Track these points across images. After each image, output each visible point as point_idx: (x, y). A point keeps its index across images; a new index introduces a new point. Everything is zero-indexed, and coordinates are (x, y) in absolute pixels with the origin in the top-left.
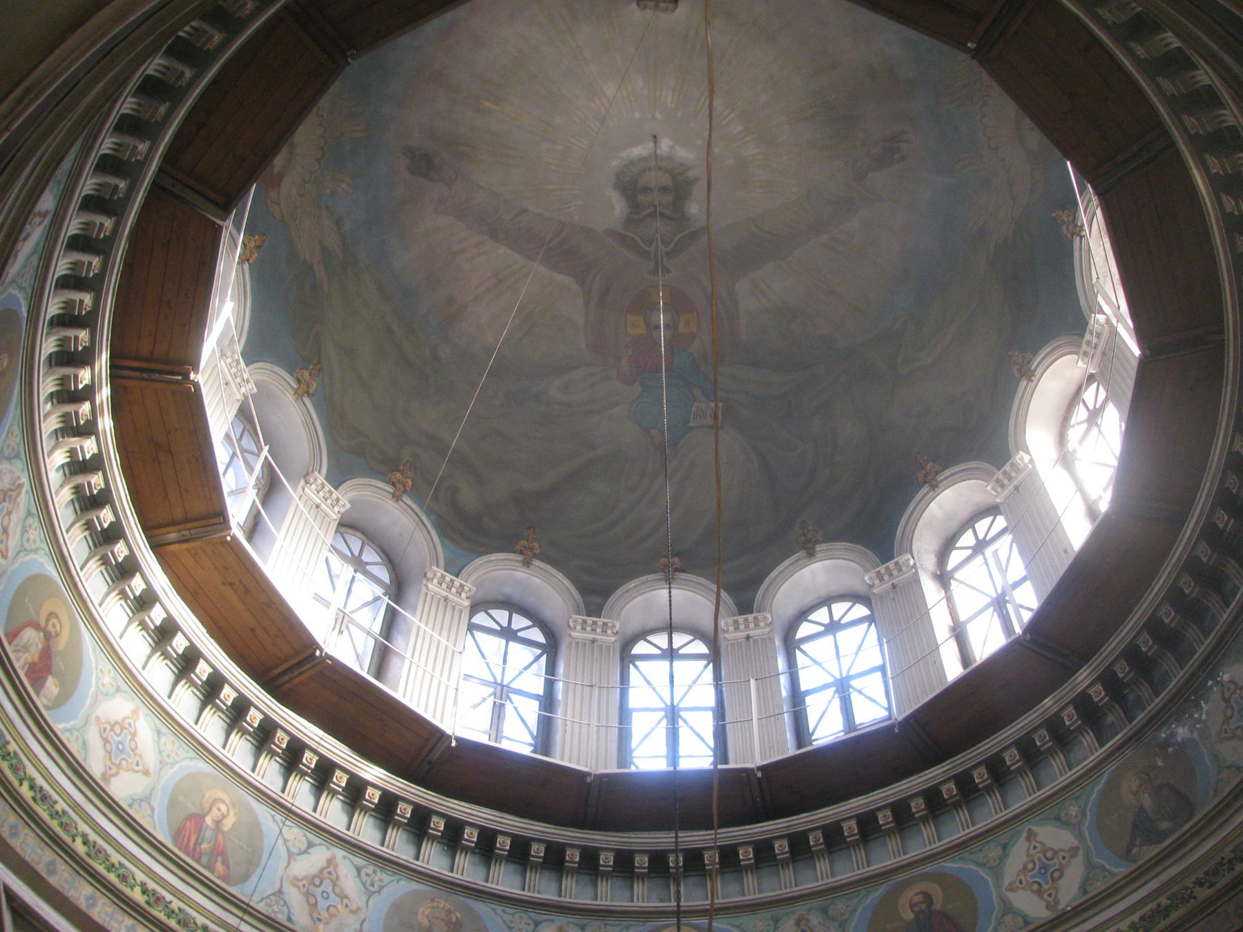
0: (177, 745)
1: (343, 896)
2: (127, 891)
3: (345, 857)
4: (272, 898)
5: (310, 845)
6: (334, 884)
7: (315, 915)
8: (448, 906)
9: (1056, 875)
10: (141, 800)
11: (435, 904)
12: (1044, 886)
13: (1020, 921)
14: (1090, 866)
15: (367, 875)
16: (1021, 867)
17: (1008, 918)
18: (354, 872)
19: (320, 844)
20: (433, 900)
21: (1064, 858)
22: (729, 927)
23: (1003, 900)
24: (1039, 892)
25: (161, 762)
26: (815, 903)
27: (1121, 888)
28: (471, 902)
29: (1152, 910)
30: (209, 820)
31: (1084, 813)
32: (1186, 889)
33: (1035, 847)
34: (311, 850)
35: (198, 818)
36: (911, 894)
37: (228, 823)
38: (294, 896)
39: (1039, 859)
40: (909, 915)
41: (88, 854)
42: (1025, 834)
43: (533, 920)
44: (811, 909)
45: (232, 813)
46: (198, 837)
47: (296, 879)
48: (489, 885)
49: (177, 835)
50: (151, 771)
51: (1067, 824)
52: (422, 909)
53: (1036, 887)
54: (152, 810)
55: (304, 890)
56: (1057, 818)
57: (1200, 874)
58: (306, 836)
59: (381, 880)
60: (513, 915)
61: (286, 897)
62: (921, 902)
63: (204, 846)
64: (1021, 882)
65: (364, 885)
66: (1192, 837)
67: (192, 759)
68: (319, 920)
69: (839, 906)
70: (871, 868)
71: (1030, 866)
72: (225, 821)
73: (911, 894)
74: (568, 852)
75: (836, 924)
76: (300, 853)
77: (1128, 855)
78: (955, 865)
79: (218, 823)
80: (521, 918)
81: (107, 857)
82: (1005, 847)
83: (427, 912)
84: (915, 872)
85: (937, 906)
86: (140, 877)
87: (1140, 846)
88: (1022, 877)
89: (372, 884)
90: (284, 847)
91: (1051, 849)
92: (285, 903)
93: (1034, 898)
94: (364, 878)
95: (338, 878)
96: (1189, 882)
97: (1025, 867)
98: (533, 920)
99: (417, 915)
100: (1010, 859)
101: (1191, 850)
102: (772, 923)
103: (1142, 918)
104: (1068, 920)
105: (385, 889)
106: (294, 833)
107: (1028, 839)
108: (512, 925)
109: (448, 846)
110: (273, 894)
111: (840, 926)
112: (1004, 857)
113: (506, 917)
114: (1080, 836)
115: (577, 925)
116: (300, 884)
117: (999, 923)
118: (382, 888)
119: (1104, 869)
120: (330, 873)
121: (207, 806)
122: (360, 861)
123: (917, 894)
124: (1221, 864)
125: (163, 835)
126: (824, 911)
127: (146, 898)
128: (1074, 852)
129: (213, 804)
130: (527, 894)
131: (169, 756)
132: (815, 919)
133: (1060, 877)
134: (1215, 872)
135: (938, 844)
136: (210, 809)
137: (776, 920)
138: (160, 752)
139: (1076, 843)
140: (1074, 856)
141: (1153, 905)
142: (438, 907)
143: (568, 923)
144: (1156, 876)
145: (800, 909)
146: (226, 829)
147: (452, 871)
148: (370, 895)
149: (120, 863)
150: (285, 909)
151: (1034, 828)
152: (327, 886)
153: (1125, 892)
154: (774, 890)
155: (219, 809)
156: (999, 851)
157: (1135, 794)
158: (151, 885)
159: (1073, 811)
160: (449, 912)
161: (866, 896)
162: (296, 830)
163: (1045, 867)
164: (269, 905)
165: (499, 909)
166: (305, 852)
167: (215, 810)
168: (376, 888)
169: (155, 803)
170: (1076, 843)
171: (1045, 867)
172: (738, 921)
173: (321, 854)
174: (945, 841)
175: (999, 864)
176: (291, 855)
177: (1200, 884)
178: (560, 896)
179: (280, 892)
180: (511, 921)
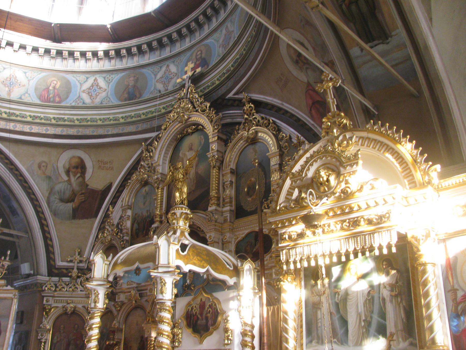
0: (33, 73)
2: (25, 120)
5: (87, 78)
6: (97, 86)
8: (134, 75)
10: (24, 94)
18: (103, 79)
25: (28, 80)
30: (51, 88)
34: (88, 80)
35: (47, 89)
37: (58, 86)
41: (8, 116)
45: (58, 82)
46: (48, 94)
49: (40, 97)
63: (51, 96)
65: (107, 82)
67: (40, 74)
70: (171, 53)
72: (56, 86)
76: (85, 82)
79: (54, 88)
80: (156, 68)
81: (15, 114)
86: (28, 114)
90: (79, 83)
92: (81, 99)
95: (98, 84)
121: (49, 85)
125: (38, 102)
127: (32, 118)
129: (51, 83)
131: (31, 77)
136: (50, 85)
138: (27, 78)
152: (95, 87)
155: (54, 83)
162: (82, 76)
165: (150, 68)
166: (86, 81)
170: (106, 88)
174: (162, 57)
176: (81, 85)
179: (79, 96)
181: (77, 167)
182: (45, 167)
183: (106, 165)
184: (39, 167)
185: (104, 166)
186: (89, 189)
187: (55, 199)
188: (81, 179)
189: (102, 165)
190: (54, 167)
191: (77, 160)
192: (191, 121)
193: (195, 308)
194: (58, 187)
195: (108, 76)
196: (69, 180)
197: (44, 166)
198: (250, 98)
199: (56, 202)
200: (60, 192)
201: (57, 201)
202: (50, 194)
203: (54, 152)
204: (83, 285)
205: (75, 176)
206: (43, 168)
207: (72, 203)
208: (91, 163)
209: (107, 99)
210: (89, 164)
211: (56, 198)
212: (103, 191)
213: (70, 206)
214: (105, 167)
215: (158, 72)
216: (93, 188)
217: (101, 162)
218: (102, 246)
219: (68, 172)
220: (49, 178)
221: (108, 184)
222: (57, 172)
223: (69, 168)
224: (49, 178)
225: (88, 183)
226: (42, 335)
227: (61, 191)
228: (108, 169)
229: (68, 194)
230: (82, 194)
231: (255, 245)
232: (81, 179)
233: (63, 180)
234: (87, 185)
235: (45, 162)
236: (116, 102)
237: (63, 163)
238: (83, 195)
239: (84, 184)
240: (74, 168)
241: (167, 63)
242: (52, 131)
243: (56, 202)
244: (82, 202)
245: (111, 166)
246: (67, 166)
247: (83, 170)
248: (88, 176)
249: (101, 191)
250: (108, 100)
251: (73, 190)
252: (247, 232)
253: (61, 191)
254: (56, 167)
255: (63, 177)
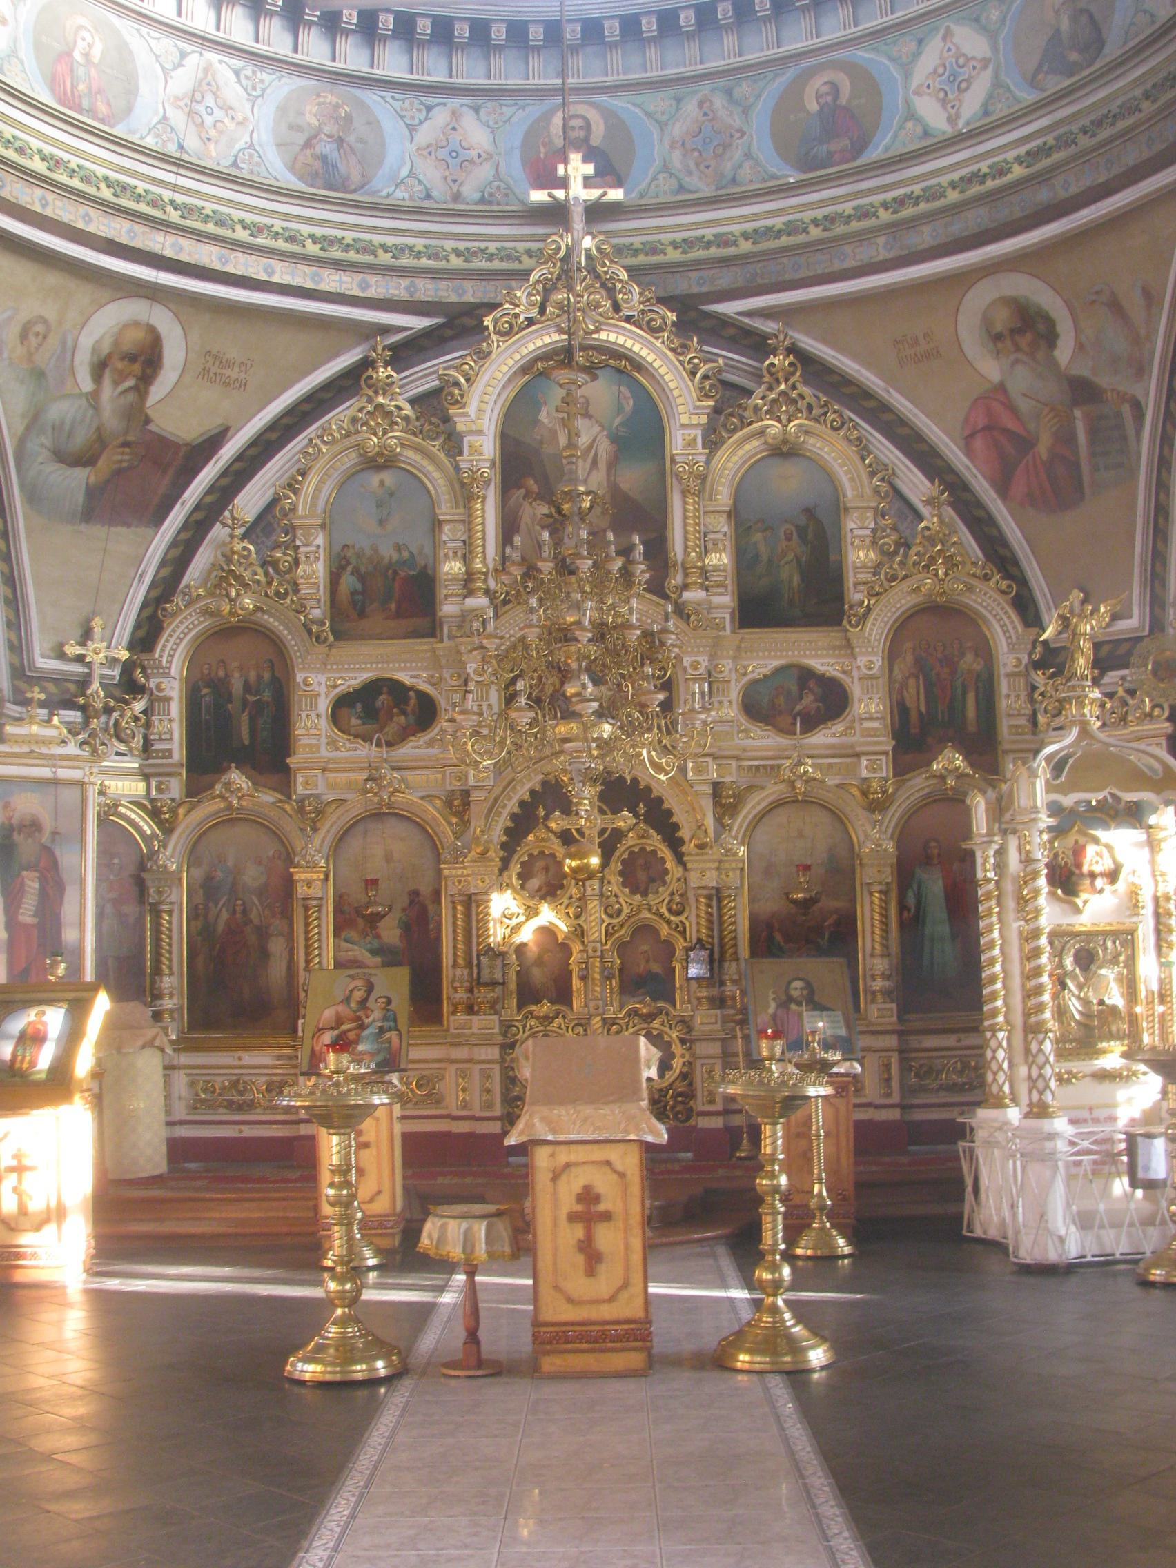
1: (227, 108)
3: (220, 62)
4: (159, 126)
5: (183, 55)
7: (204, 135)
8: (335, 100)
9: (964, 85)
10: (9, 56)
11: (322, 100)
12: (951, 96)
13: (919, 130)
14: (997, 84)
15: (247, 78)
16: (931, 70)
17: (909, 125)
19: (194, 52)
20: (318, 95)
21: (974, 68)
22: (629, 106)
23: (907, 103)
24: (944, 102)
26: (720, 83)
27: (1016, 119)
28: (358, 92)
29: (1038, 147)
30: (77, 56)
31: (1003, 21)
32: (1072, 133)
33: (949, 50)
36: (818, 83)
38: (178, 118)
39: (940, 83)
40: (813, 107)
42: (942, 31)
43: (424, 104)
44: (716, 89)
45: (97, 39)
47: (177, 99)
48: (375, 71)
50: (7, 17)
51: (984, 29)
52: (308, 108)
53: (942, 95)
54: (22, 63)
55: (187, 110)
56: (977, 20)
57: (1086, 122)
58: (176, 46)
59: (262, 81)
60: (403, 100)
61: (172, 122)
62: (827, 94)
64: (928, 87)
65: (246, 90)
66: (1091, 81)
68: (209, 140)
69: (743, 90)
71: (941, 70)
73: (818, 83)
74: (457, 26)
75: (740, 109)
76: (175, 68)
77: (1033, 83)
78: (866, 55)
80: (412, 104)
82: (920, 42)
83: (314, 111)
84: (824, 58)
85: (843, 100)
87: (1047, 73)
88: (930, 82)
89: (254, 89)
91: (964, 55)
93: (937, 107)
94: (244, 82)
95: (218, 88)
96: (1074, 128)
97: (935, 71)
98: (424, 104)
99: (304, 115)
100: (923, 57)
101: (1087, 94)
102: (674, 103)
103: (1028, 153)
104: (962, 141)
105: (268, 91)
106: (167, 45)
107: (944, 39)
108: (403, 113)
109: (326, 28)
110: (159, 122)
111: (743, 112)
112: (917, 55)
113: (397, 105)
114: (995, 48)
115: (470, 107)
116: (182, 104)
117: (901, 128)
118: (264, 90)
119: (1009, 89)
120: (209, 84)
122: (237, 63)
123: (826, 83)
124: (1106, 116)
126: (729, 92)
128: (985, 63)
130: (417, 77)
132: (719, 102)
133: (967, 89)
134: (1099, 123)
135: (853, 30)
136: (75, 42)
137: (679, 100)
139: (989, 54)
140: (985, 68)
141: (1039, 142)
142: (324, 103)
143: (462, 105)
144: (1050, 112)
145: (705, 88)
146: (96, 60)
147: (334, 60)
148: (253, 100)
149: (14, 137)
150: (174, 135)
151: (953, 27)
153: (1020, 122)
154: (677, 66)
155: (84, 39)
156: (913, 45)
157: (1057, 12)
158: (48, 149)
159: (995, 15)
160: (337, 106)
161: (774, 79)
163: (954, 75)
164: (157, 136)
165: (388, 95)
166: (180, 65)
167: (79, 42)
168: (259, 92)
169: (22, 55)
170: (989, 54)
171: (954, 75)
172: (638, 99)
173: (197, 59)
175: (911, 63)
177: (1084, 131)
178: (451, 77)
179: (165, 118)
180: (402, 109)
181: (132, 358)
182: (40, 337)
183: (227, 372)
184: (24, 336)
185: (219, 371)
186: (151, 432)
187: (40, 445)
188: (131, 397)
189: (215, 369)
190: (64, 343)
191: (139, 335)
192: (598, 340)
193: (1061, 856)
194: (61, 410)
195: (249, 72)
196: (95, 395)
197: (37, 334)
198: (793, 344)
199: (40, 459)
200: (57, 428)
201: (44, 454)
202: (28, 429)
203: (83, 294)
204: (123, 736)
205: (116, 383)
206: (33, 341)
207: (88, 469)
208: (183, 354)
209: (251, 156)
210: (174, 354)
211: (42, 445)
212: (194, 447)
213: (80, 476)
214: (221, 375)
215: (421, 123)
216: (164, 434)
217: (215, 357)
218: (200, 623)
219: (100, 368)
220: (39, 375)
221: (217, 431)
222: (68, 362)
223: (109, 356)
224: (39, 375)
225: (149, 412)
226: (160, 893)
227: (62, 423)
228: (229, 384)
229: (81, 438)
230: (126, 444)
231: (801, 698)
232: (131, 397)
233: (78, 391)
234: (148, 421)
235: (45, 321)
236: (277, 169)
237: (96, 336)
238: (127, 450)
239: (136, 414)
240: (122, 359)
241: (454, 102)
242: (102, 227)
243: (40, 459)
244: (118, 473)
245: (242, 376)
246: (106, 348)
247: (148, 371)
248: (158, 391)
249: (187, 445)
250: (256, 159)
251: (98, 429)
252: (776, 663)
253: (62, 423)
254: (70, 343)
255: (79, 381)
